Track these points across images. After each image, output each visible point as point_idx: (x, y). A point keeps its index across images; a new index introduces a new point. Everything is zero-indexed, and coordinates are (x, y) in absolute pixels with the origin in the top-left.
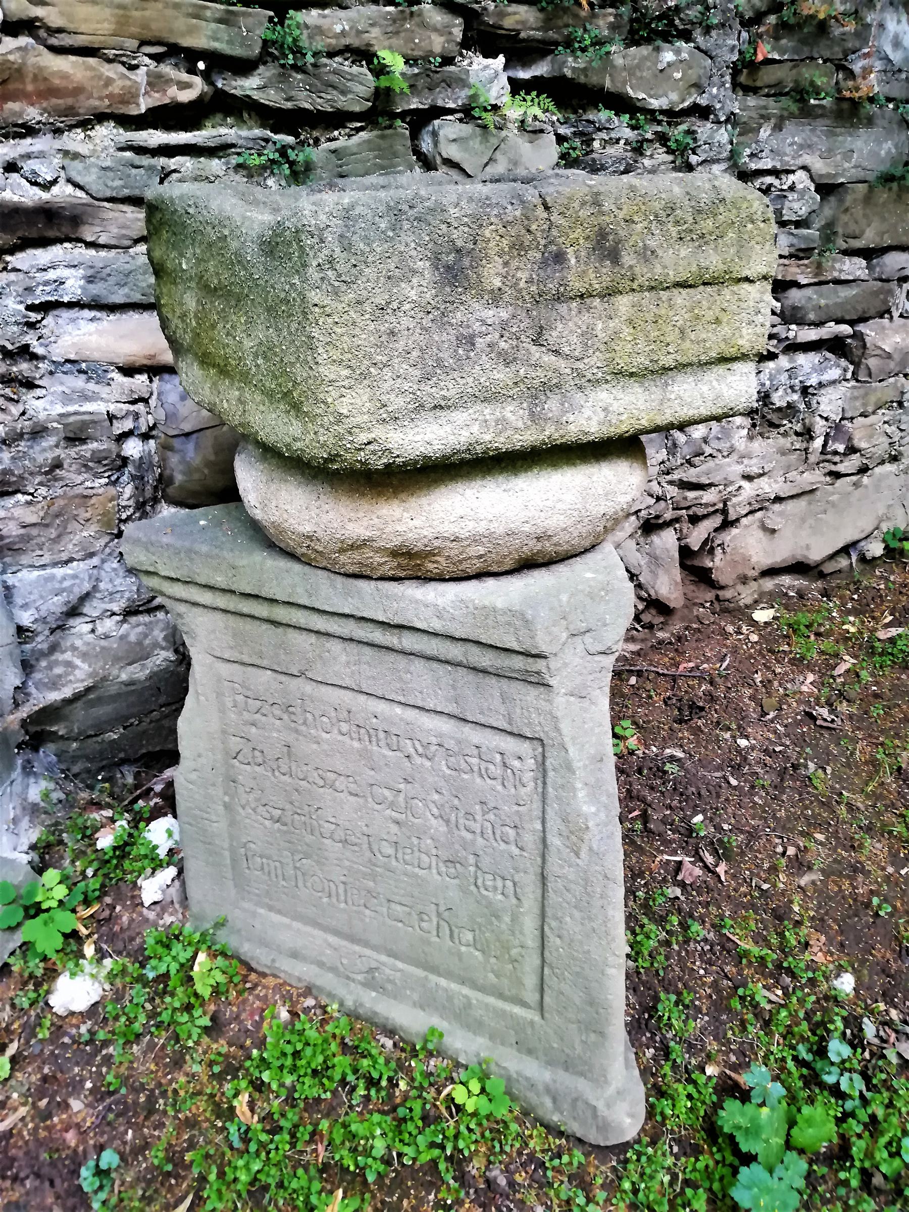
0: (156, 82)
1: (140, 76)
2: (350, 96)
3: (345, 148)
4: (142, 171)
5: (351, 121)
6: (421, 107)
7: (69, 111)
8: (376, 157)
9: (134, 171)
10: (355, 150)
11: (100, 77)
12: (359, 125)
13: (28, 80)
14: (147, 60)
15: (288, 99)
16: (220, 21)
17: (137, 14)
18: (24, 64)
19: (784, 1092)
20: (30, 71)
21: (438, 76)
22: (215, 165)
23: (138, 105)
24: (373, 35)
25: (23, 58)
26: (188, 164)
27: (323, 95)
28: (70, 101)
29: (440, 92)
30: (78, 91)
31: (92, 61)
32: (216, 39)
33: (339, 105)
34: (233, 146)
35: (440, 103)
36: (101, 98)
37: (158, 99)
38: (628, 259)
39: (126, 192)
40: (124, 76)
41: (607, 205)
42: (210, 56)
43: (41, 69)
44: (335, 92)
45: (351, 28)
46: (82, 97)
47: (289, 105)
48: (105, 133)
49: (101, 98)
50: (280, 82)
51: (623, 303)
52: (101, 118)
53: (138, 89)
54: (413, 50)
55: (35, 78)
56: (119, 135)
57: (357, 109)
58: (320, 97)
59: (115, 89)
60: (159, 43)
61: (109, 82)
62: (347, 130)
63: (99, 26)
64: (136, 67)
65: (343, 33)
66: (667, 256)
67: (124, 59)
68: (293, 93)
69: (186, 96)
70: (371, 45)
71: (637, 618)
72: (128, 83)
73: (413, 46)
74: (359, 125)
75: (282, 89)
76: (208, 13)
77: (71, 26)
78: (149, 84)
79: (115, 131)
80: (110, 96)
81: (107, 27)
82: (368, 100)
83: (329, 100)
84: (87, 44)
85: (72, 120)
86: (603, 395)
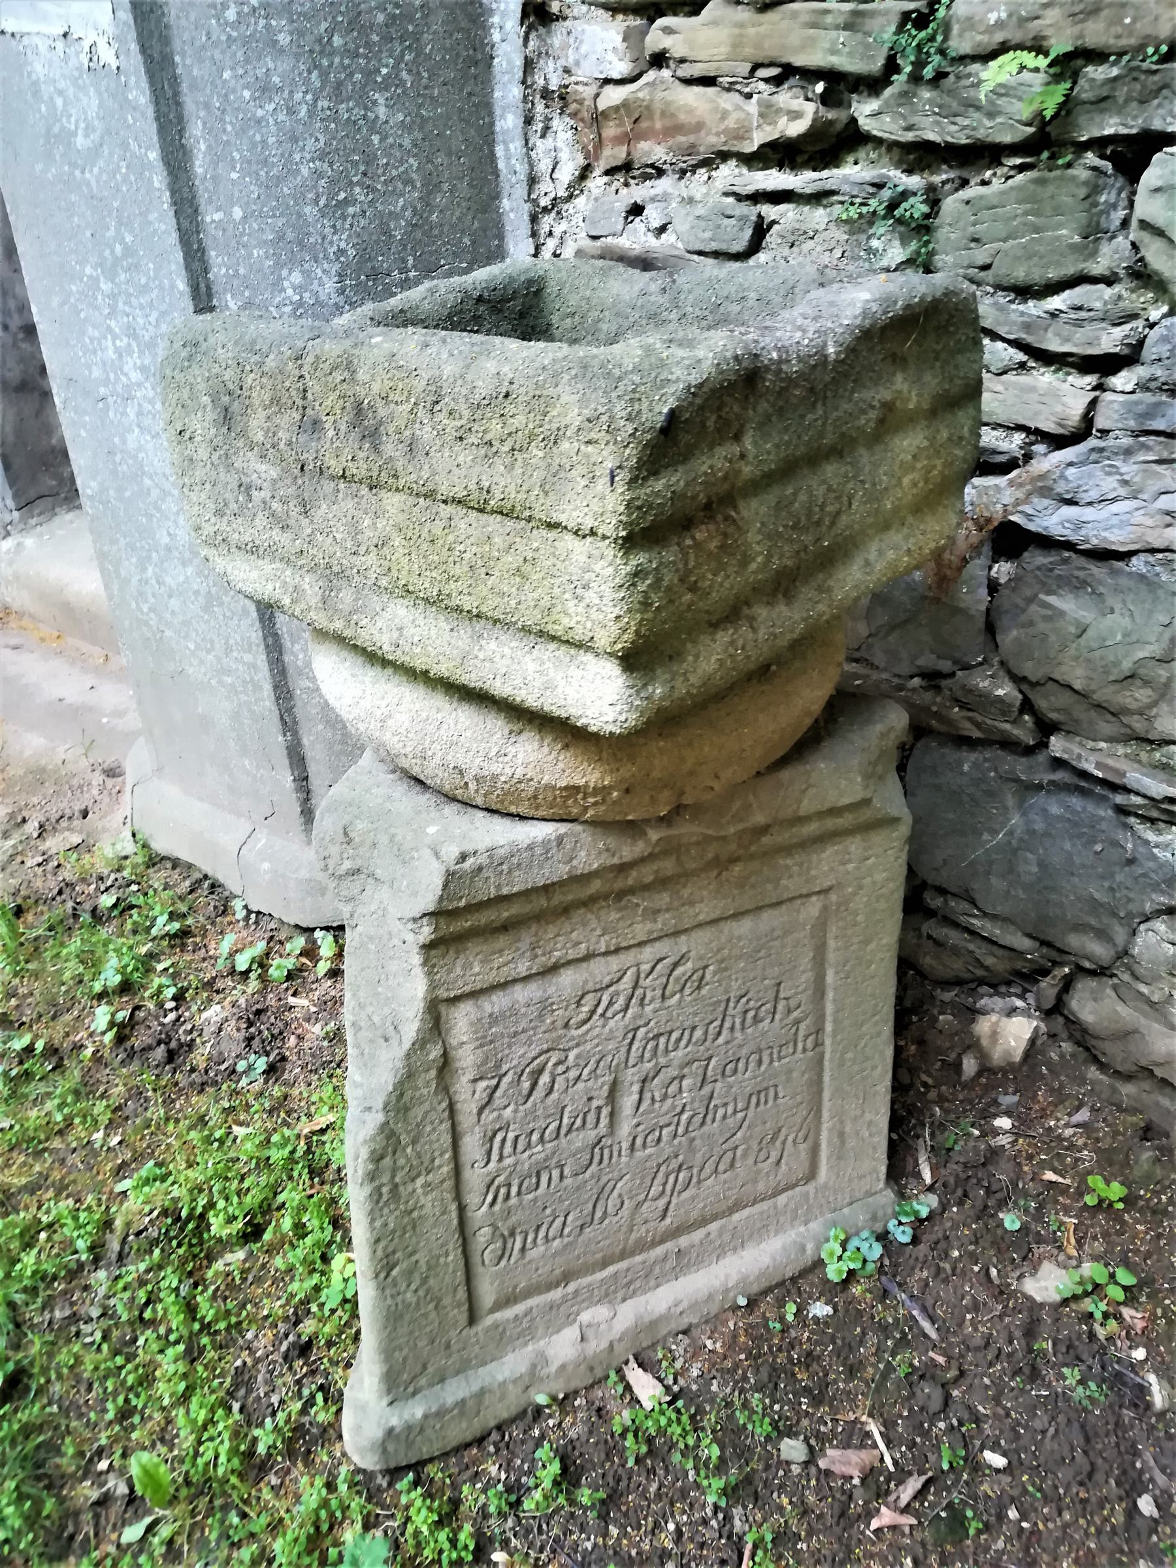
0: (768, 113)
1: (752, 107)
2: (999, 120)
3: (981, 197)
4: (733, 221)
5: (1009, 156)
6: (1125, 131)
7: (691, 150)
8: (1026, 213)
9: (726, 221)
10: (995, 202)
11: (716, 109)
12: (1018, 161)
13: (657, 116)
14: (762, 86)
15: (909, 128)
16: (848, 27)
17: (752, 31)
18: (651, 100)
19: (127, 1491)
20: (658, 106)
21: (1156, 78)
22: (818, 216)
23: (752, 141)
24: (1048, 22)
25: (651, 93)
26: (790, 214)
27: (959, 119)
28: (691, 138)
29: (1159, 106)
30: (699, 127)
31: (711, 91)
32: (834, 52)
33: (981, 134)
34: (832, 193)
35: (1157, 125)
36: (718, 134)
37: (770, 134)
38: (389, 448)
39: (714, 246)
40: (738, 108)
41: (362, 375)
42: (832, 77)
43: (668, 104)
44: (976, 115)
45: (1010, 16)
46: (703, 133)
47: (910, 136)
48: (728, 173)
49: (718, 134)
50: (900, 105)
51: (393, 502)
52: (724, 156)
53: (751, 122)
54: (1118, 37)
55: (663, 114)
56: (741, 175)
57: (1007, 138)
58: (954, 123)
59: (731, 123)
60: (771, 64)
61: (725, 115)
62: (1006, 169)
63: (715, 51)
64: (749, 96)
65: (1000, 24)
66: (442, 460)
67: (738, 87)
68: (915, 119)
69: (796, 128)
70: (1044, 38)
71: (206, 877)
72: (743, 115)
73: (1119, 30)
74: (1018, 161)
75: (901, 115)
76: (829, 19)
77: (690, 55)
78: (761, 115)
79: (737, 171)
80: (725, 131)
81: (724, 50)
82: (1029, 124)
83: (964, 128)
84: (704, 73)
85: (693, 160)
86: (400, 611)
